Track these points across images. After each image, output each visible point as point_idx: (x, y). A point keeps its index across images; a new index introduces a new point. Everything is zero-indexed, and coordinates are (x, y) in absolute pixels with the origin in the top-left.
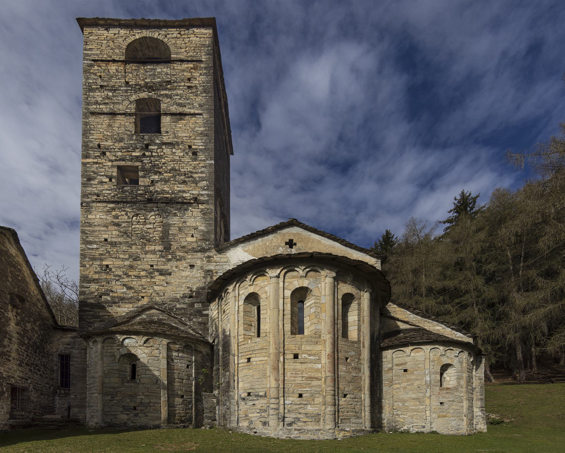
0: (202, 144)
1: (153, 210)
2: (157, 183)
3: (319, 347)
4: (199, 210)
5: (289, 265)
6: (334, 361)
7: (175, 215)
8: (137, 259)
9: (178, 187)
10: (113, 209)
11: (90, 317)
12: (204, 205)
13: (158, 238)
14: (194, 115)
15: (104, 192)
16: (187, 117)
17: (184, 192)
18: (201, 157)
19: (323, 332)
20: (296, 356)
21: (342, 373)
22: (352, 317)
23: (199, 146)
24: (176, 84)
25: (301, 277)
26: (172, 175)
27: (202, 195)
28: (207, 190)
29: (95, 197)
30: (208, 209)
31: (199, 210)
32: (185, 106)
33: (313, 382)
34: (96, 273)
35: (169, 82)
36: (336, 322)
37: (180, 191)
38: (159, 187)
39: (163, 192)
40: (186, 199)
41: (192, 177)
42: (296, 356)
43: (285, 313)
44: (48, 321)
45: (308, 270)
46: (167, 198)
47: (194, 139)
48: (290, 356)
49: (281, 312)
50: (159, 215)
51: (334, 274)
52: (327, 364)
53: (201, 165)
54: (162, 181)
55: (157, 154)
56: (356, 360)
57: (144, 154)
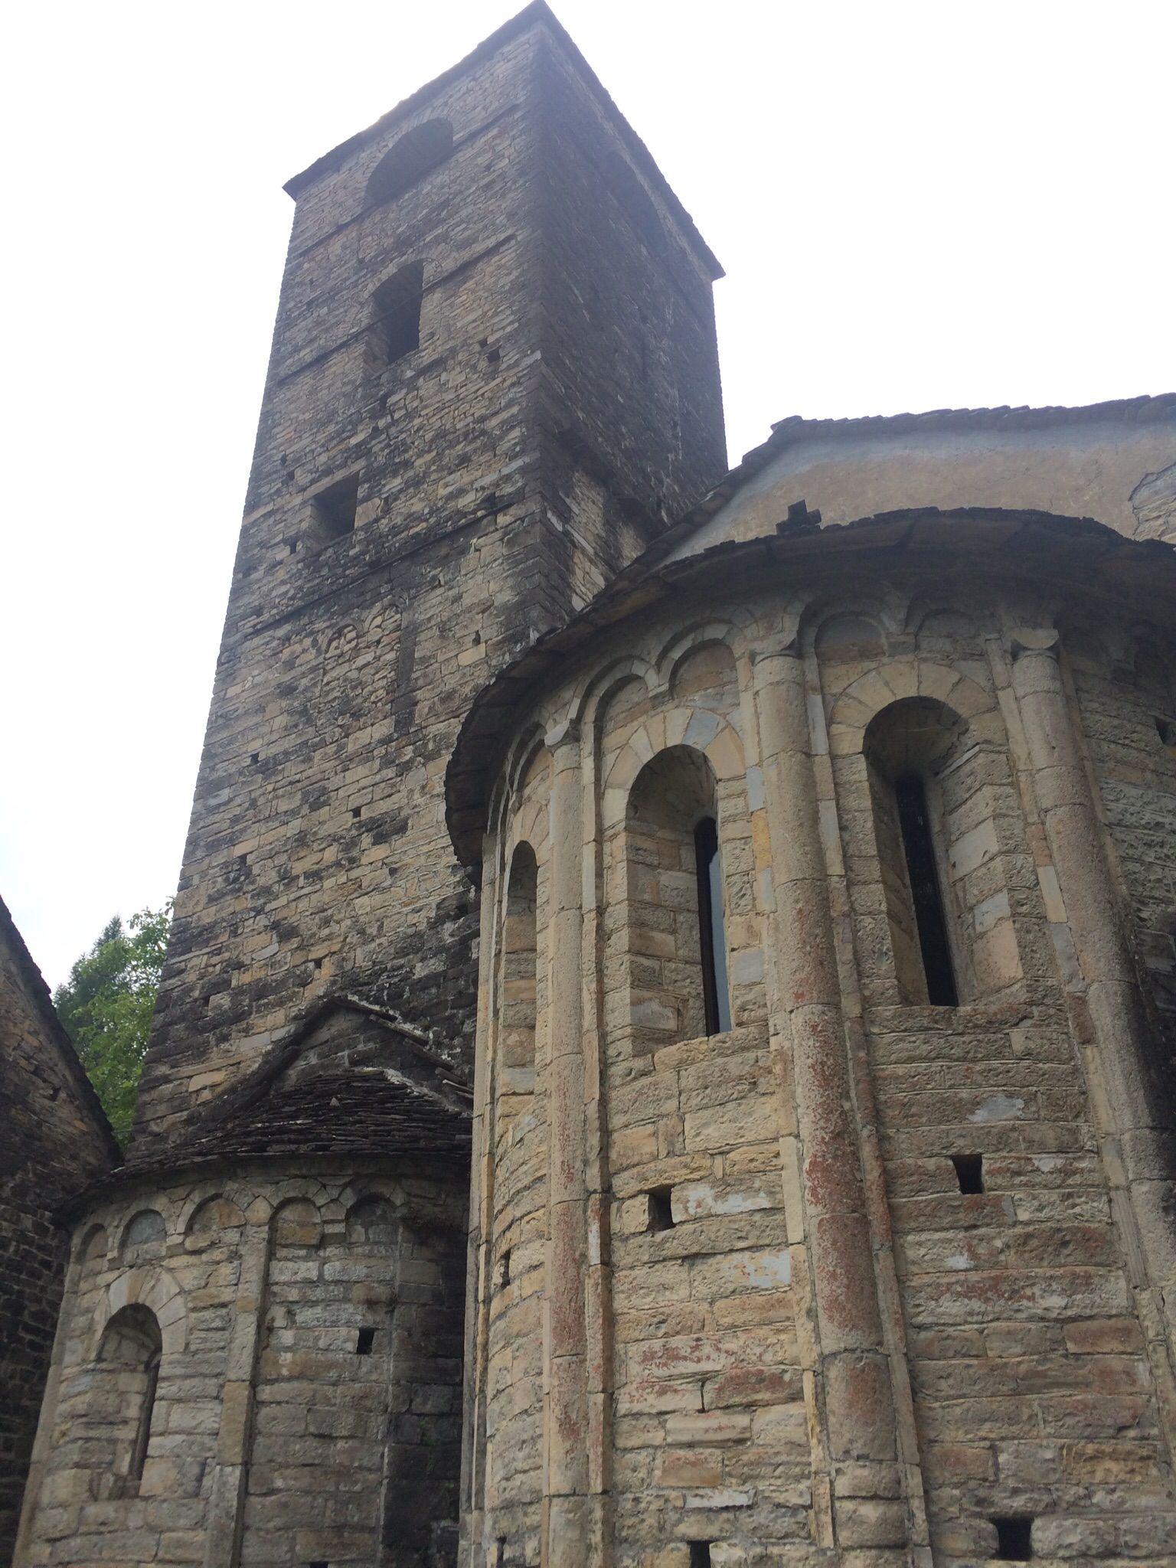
0: (511, 318)
1: (378, 597)
2: (395, 500)
3: (765, 1115)
4: (498, 535)
5: (605, 663)
6: (860, 1204)
7: (434, 584)
8: (317, 799)
9: (446, 485)
10: (286, 639)
11: (162, 1109)
12: (512, 510)
13: (381, 693)
14: (490, 252)
15: (274, 594)
16: (480, 266)
17: (461, 492)
18: (510, 357)
19: (773, 994)
20: (660, 1202)
21: (951, 1307)
22: (974, 846)
23: (503, 328)
24: (458, 199)
25: (657, 701)
26: (434, 453)
27: (507, 478)
28: (523, 452)
29: (253, 620)
30: (522, 520)
31: (498, 535)
32: (475, 240)
33: (765, 1418)
34: (212, 900)
35: (446, 203)
36: (839, 906)
37: (451, 497)
38: (402, 508)
39: (413, 518)
40: (465, 515)
41: (483, 433)
42: (660, 1202)
43: (609, 923)
44: (74, 1157)
45: (676, 654)
46: (418, 534)
47: (496, 314)
48: (634, 1215)
49: (590, 924)
50: (392, 605)
51: (788, 629)
52: (814, 1241)
53: (508, 383)
54: (408, 488)
55: (403, 412)
56: (1047, 1163)
57: (376, 429)
